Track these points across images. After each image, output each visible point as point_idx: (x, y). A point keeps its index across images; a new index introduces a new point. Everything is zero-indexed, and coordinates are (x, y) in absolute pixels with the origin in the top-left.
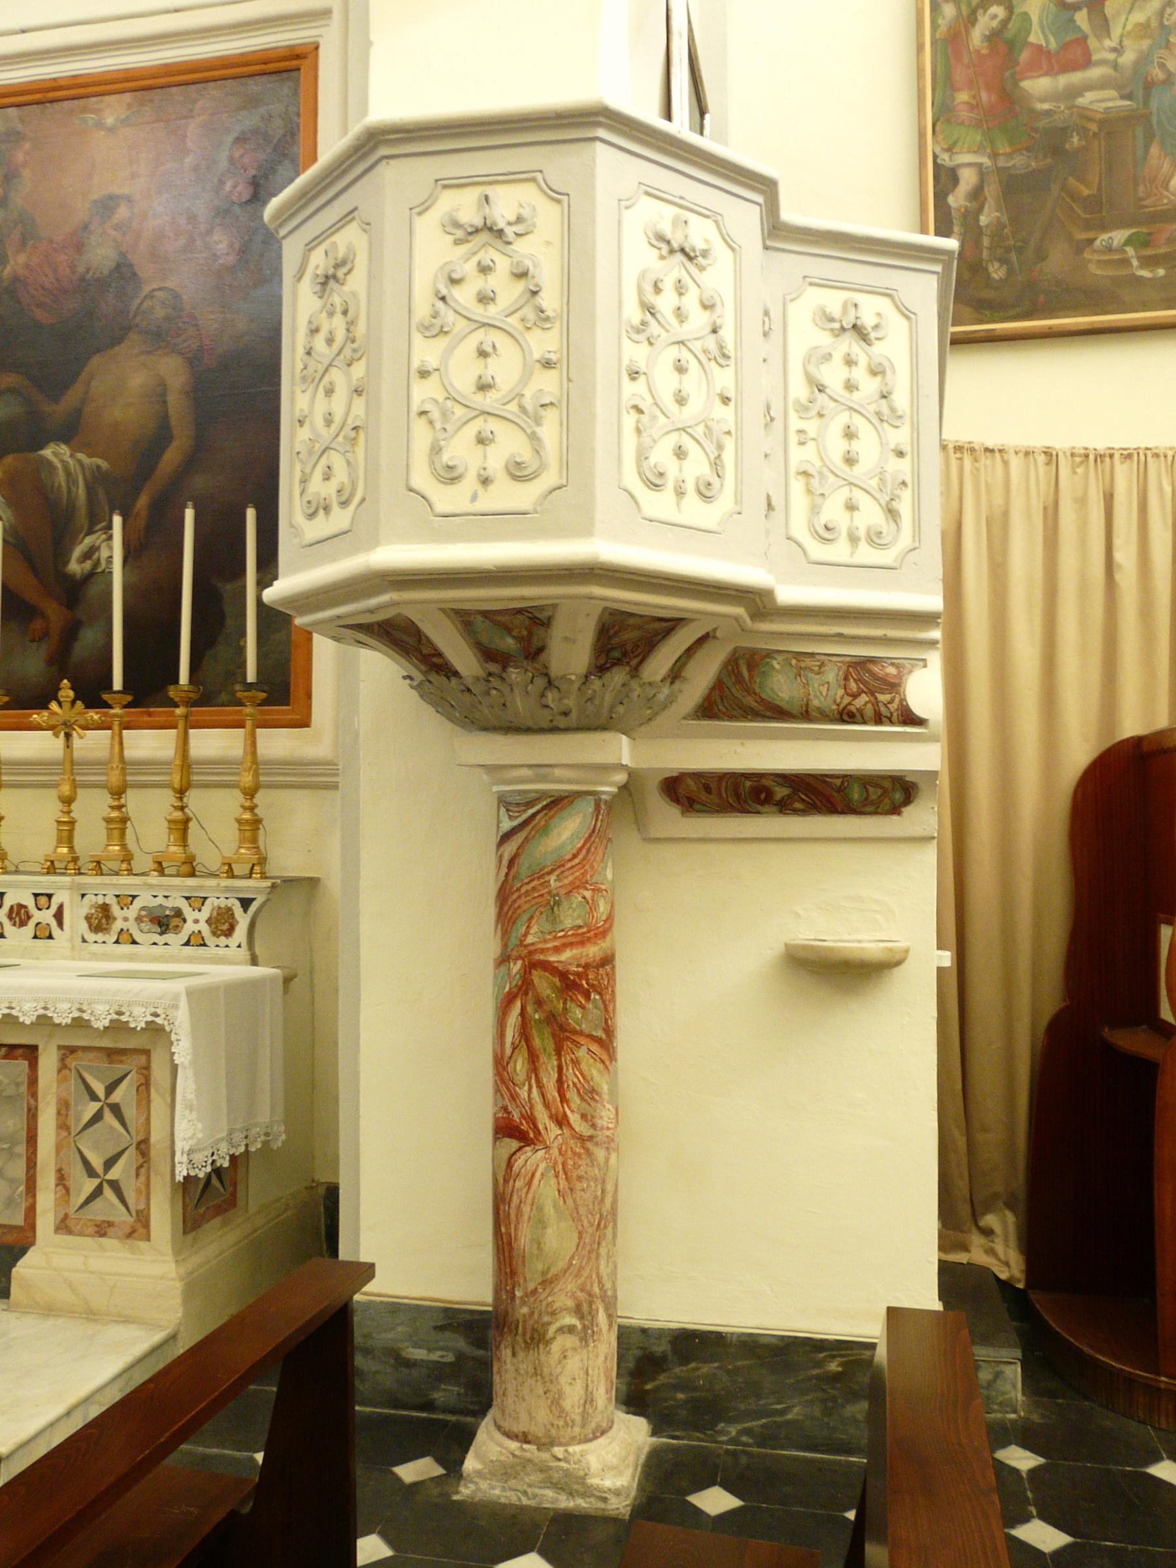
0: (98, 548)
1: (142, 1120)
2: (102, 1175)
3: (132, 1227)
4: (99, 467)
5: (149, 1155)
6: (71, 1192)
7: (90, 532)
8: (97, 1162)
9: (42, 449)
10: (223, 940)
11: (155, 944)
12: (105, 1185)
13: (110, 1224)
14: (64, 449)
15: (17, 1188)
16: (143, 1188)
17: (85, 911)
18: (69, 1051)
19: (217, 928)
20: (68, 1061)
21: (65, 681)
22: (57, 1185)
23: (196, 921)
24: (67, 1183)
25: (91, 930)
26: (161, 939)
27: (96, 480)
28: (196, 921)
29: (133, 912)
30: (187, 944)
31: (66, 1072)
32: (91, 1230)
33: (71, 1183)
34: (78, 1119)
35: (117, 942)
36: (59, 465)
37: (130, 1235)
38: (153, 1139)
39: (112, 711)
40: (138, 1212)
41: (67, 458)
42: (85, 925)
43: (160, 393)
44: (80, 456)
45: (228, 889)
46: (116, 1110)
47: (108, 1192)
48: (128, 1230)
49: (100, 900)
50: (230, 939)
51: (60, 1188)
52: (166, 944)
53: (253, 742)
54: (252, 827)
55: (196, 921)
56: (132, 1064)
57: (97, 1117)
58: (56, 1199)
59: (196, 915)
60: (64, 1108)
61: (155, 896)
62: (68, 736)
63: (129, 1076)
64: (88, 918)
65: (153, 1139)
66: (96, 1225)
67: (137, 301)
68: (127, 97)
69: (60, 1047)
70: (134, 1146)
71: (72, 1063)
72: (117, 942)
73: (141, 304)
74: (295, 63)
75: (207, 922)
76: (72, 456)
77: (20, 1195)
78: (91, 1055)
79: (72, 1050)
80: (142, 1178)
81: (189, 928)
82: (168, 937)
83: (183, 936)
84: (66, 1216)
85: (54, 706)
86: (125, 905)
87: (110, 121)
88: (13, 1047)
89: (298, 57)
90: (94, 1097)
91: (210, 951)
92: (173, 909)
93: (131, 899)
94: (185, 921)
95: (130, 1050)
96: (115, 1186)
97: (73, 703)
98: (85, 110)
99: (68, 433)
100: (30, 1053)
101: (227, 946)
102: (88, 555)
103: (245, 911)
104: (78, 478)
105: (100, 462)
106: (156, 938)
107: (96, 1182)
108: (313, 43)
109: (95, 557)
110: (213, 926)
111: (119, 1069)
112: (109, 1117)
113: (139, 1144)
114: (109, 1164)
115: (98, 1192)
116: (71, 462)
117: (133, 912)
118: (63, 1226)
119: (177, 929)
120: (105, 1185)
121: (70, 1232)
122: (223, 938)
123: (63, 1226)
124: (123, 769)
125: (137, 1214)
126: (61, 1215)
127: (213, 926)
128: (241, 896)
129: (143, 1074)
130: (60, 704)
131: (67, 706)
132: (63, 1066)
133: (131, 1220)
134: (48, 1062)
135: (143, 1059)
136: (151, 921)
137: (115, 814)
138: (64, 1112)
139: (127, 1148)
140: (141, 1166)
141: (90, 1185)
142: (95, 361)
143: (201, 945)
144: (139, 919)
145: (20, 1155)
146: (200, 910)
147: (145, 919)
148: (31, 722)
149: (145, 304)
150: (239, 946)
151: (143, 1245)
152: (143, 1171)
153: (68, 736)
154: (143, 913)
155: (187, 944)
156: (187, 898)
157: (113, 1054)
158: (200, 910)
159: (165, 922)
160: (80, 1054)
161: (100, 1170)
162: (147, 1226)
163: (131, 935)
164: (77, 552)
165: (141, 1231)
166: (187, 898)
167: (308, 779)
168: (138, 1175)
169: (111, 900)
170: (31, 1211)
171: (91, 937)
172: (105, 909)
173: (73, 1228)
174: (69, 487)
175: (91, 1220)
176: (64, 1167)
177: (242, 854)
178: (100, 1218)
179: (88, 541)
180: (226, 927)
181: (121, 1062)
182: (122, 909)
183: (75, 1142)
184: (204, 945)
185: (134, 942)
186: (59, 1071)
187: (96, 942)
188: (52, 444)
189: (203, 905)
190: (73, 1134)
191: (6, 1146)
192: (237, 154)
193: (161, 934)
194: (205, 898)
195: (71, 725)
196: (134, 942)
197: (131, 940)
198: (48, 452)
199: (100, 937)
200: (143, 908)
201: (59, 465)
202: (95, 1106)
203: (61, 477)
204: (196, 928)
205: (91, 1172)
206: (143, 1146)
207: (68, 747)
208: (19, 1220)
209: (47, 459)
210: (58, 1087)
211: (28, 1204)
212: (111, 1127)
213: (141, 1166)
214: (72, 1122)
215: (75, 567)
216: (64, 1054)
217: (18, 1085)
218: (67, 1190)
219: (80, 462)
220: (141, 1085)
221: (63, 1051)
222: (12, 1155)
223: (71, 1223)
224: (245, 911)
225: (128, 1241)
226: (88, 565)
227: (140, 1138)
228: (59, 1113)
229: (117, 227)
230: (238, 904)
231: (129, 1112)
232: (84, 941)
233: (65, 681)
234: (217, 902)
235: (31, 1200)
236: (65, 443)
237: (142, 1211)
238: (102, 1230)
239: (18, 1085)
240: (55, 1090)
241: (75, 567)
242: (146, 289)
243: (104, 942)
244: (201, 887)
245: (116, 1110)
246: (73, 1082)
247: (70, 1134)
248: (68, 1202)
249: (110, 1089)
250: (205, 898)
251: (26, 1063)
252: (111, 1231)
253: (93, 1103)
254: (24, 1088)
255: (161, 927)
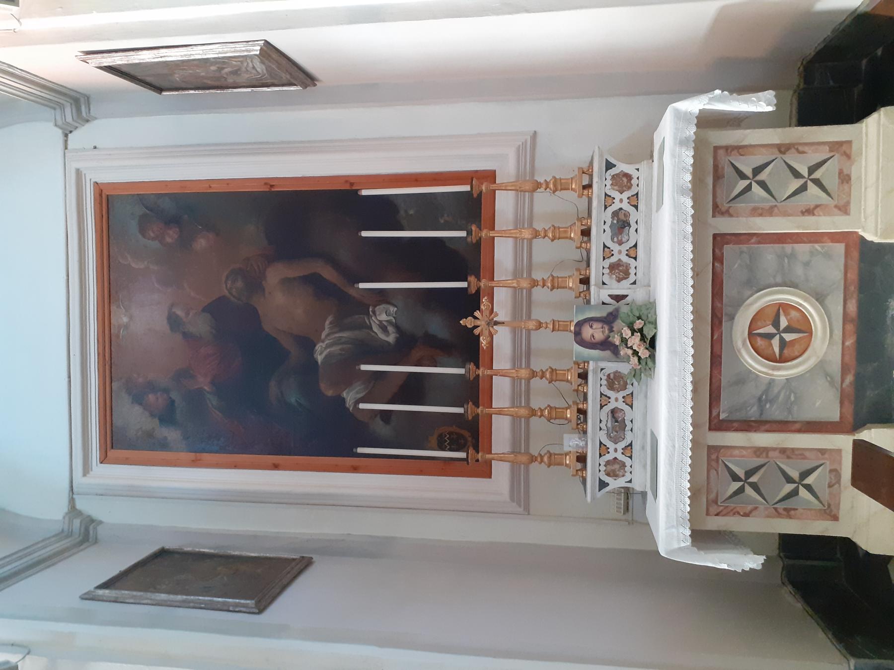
0: (380, 322)
1: (763, 150)
2: (805, 180)
3: (842, 155)
4: (331, 323)
5: (789, 144)
6: (819, 203)
7: (371, 328)
8: (796, 184)
9: (317, 362)
10: (634, 182)
11: (636, 231)
12: (812, 177)
13: (841, 172)
14: (318, 348)
15: (817, 250)
16: (813, 148)
17: (614, 282)
18: (717, 210)
19: (625, 186)
20: (724, 209)
21: (461, 322)
22: (814, 215)
23: (621, 201)
24: (812, 207)
25: (627, 278)
26: (629, 425)
27: (339, 325)
28: (621, 201)
29: (615, 247)
30: (636, 207)
31: (731, 211)
32: (846, 186)
33: (812, 204)
34: (763, 200)
35: (635, 259)
36: (328, 350)
37: (848, 156)
38: (777, 142)
39: (481, 375)
40: (831, 151)
41: (324, 345)
42: (624, 282)
43: (287, 282)
44: (323, 336)
45: (600, 178)
46: (757, 171)
47: (817, 175)
48: (844, 158)
49: (607, 271)
50: (633, 176)
51: (815, 212)
52: (637, 222)
53: (500, 412)
54: (559, 185)
55: (621, 201)
56: (724, 160)
57: (763, 185)
58: (825, 215)
59: (617, 201)
60: (758, 212)
61: (604, 231)
62: (496, 323)
63: (732, 161)
64: (619, 280)
65: (777, 141)
66: (842, 183)
67: (232, 299)
68: (113, 308)
69: (714, 216)
70: (782, 156)
71: (725, 206)
72: (635, 259)
73: (234, 297)
74: (104, 196)
75: (621, 194)
76: (323, 342)
77: (823, 247)
78: (719, 192)
79: (716, 206)
80: (806, 149)
81: (625, 206)
82: (632, 221)
83: (631, 210)
84: (836, 206)
85: (476, 332)
86: (610, 253)
87: (125, 320)
88: (715, 258)
89: (101, 195)
90: (748, 188)
91: (642, 189)
92: (613, 218)
93: (606, 249)
94: (621, 209)
95: (714, 162)
96: (812, 170)
97: (476, 318)
98: (118, 336)
99: (307, 344)
100: (720, 240)
101: (638, 178)
102: (384, 329)
103: (615, 166)
104: (335, 337)
105: (327, 322)
106: (632, 230)
107: (810, 184)
108: (94, 185)
109: (385, 323)
110: (624, 188)
111: (728, 171)
112: (762, 176)
113: (781, 152)
114: (796, 174)
115: (818, 183)
116: (327, 342)
117: (615, 247)
118: (844, 209)
119: (627, 215)
120: (812, 177)
121: (848, 203)
122: (632, 182)
123: (844, 209)
124: (517, 453)
125: (833, 151)
126: (836, 211)
127: (624, 188)
128: (604, 169)
129: (731, 152)
130: (476, 327)
131: (478, 323)
132: (727, 213)
133: (837, 156)
134: (726, 225)
135: (721, 152)
136: (621, 234)
137: (546, 459)
138: (760, 211)
139: (785, 162)
140: (797, 150)
141: (813, 189)
142: (267, 327)
143: (637, 197)
144: (620, 243)
145: (793, 248)
146: (614, 199)
147: (620, 238)
148: (487, 347)
149: (234, 293)
150: (638, 170)
151: (855, 146)
152: (801, 148)
153: (496, 323)
154: (615, 239)
155: (636, 207)
156: (606, 208)
157: (718, 176)
158: (614, 199)
159: (621, 224)
160: (718, 200)
161: (800, 182)
162: (840, 144)
163: (630, 248)
164: (382, 336)
165: (844, 148)
166: (606, 208)
167: (528, 161)
168: (804, 152)
169: (607, 263)
170: (835, 237)
171: (632, 278)
172: (613, 267)
173: (845, 201)
174: (341, 344)
175: (839, 188)
176: (800, 210)
177: (570, 461)
178: (837, 181)
179: (375, 329)
180: (625, 180)
181: (723, 168)
182: (613, 255)
183: (781, 202)
184: (637, 194)
185: (635, 246)
186: (731, 216)
187: (635, 274)
188: (315, 356)
189: (610, 196)
190: (774, 203)
191: (786, 261)
192: (152, 235)
193: (629, 226)
194: (606, 194)
195: (490, 320)
196: (635, 246)
197: (634, 248)
198: (320, 358)
199: (632, 271)
200: (612, 239)
201: (328, 350)
202: (756, 188)
203: (336, 349)
204: (626, 201)
205: (803, 188)
206: (783, 149)
207: (504, 323)
208: (840, 248)
209: (324, 358)
210: (742, 217)
211: (829, 241)
212: (770, 174)
213: (797, 150)
214: (767, 205)
215: (391, 338)
216: (719, 213)
217: (742, 252)
218: (817, 206)
219: (328, 335)
220: (738, 152)
221: (717, 213)
222: (792, 256)
223: (841, 203)
224: (615, 166)
225: (853, 157)
226: (390, 329)
227: (778, 152)
228: (761, 215)
229: (187, 314)
230: (609, 171)
231: (758, 161)
232: (634, 283)
233: (461, 322)
234: (608, 187)
235: (826, 238)
236: (315, 346)
237: (830, 148)
238: (845, 178)
239: (742, 252)
240: (744, 219)
241: (391, 338)
242: (226, 293)
243: (636, 268)
244: (599, 196)
245: (757, 171)
246: (740, 205)
247: (776, 206)
248: (826, 206)
249: (743, 176)
250: (606, 194)
251: (725, 246)
252: (846, 172)
253: (752, 189)
254: (744, 247)
255: (625, 227)
